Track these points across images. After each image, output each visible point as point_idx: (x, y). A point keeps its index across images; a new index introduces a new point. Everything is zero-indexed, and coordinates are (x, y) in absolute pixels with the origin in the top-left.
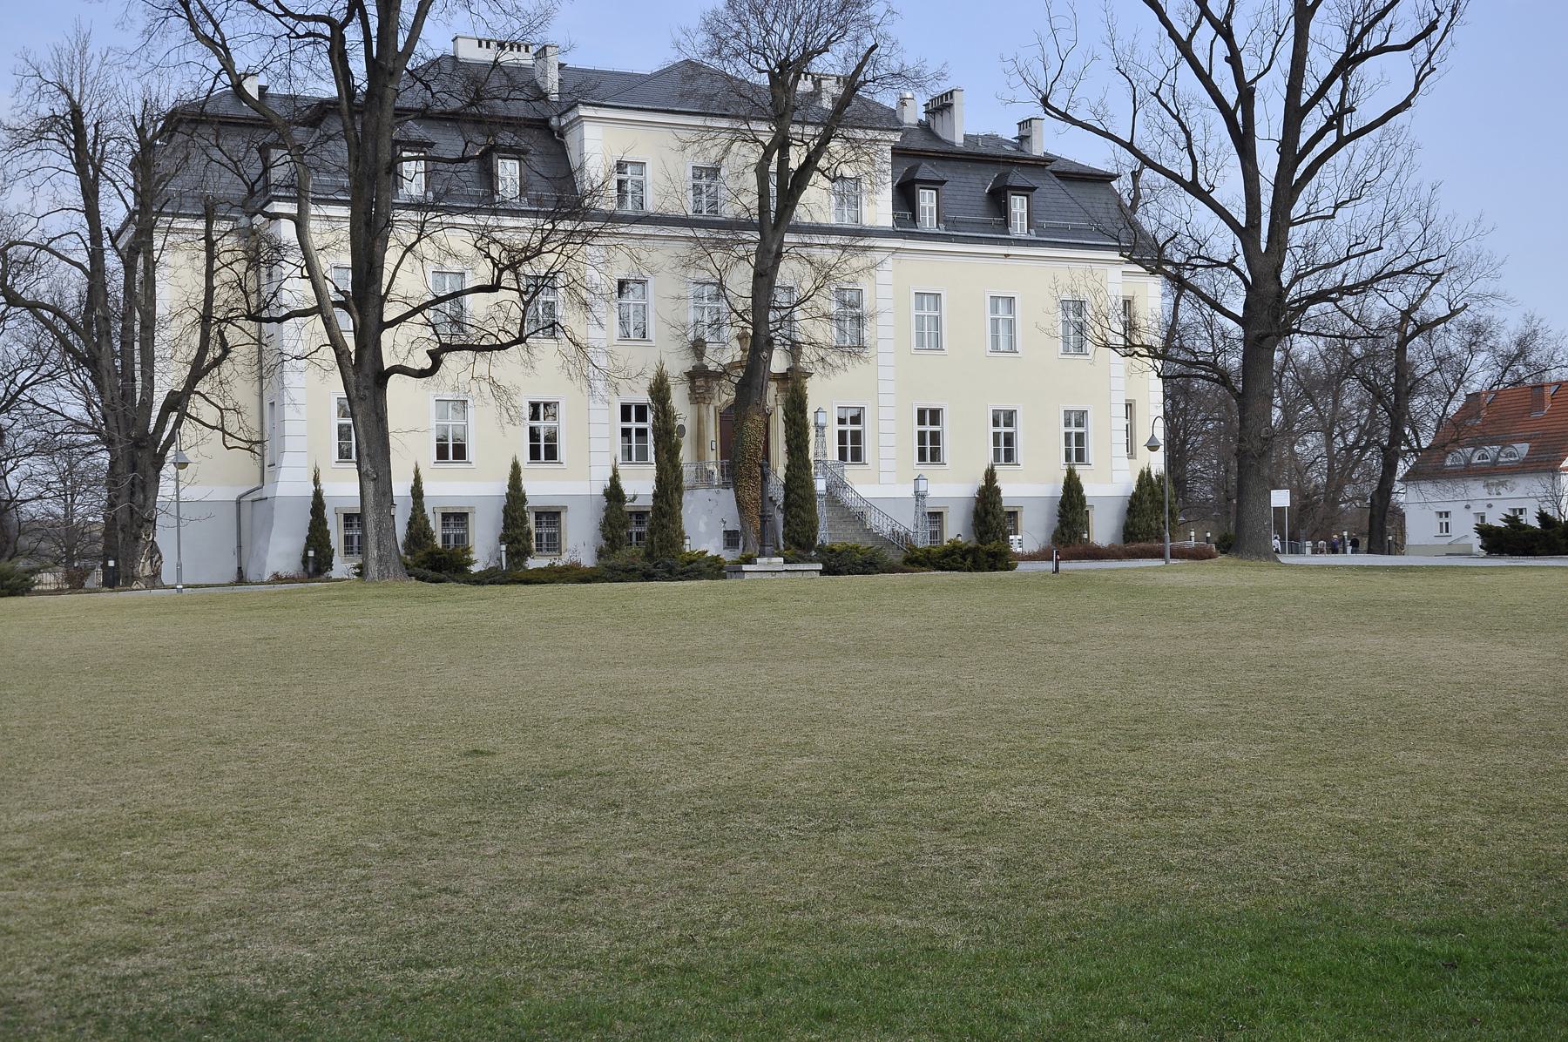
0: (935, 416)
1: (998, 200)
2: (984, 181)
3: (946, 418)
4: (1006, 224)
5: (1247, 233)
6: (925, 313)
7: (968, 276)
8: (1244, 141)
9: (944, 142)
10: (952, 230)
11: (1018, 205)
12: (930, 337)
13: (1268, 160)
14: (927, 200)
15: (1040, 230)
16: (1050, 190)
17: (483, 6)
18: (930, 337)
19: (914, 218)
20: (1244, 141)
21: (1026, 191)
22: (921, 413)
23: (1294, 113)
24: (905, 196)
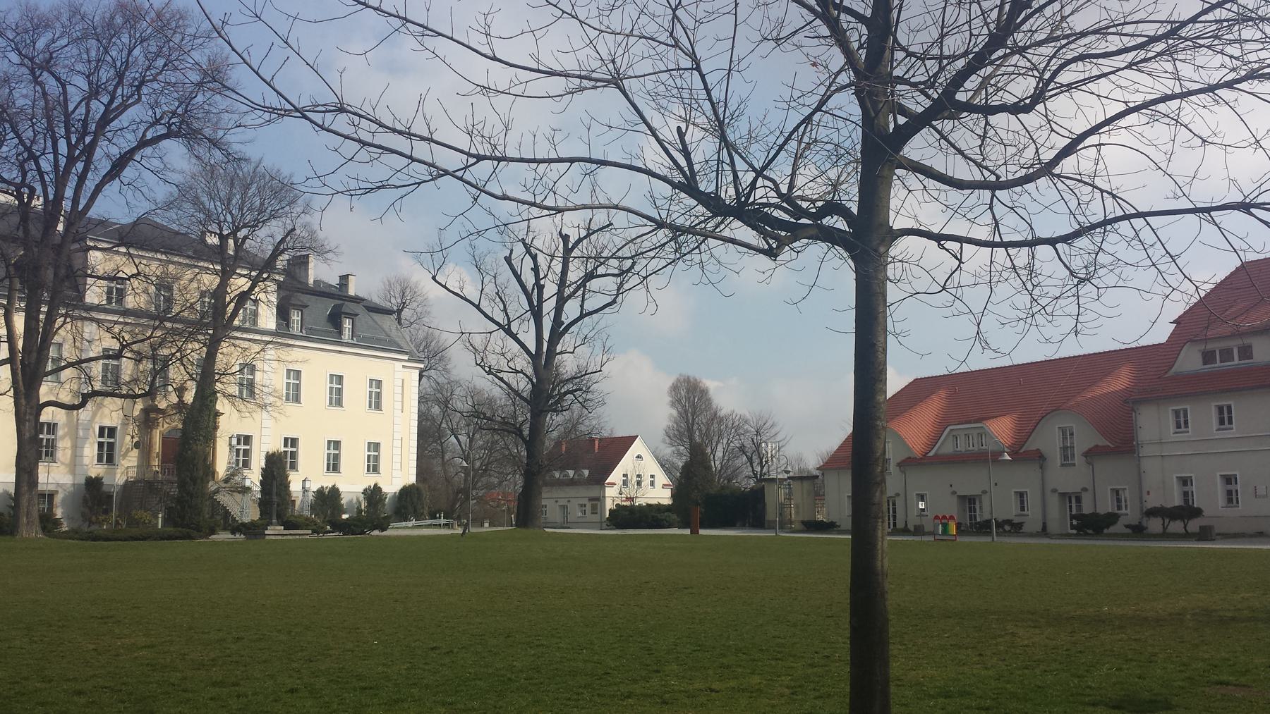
0: (377, 446)
1: (335, 320)
2: (328, 306)
3: (301, 444)
4: (340, 333)
5: (535, 358)
6: (292, 381)
7: (318, 363)
8: (537, 314)
9: (300, 282)
10: (311, 335)
11: (347, 324)
12: (337, 398)
13: (547, 324)
14: (296, 317)
15: (310, 330)
16: (364, 317)
17: (4, 149)
18: (337, 398)
19: (288, 325)
20: (537, 314)
21: (353, 316)
22: (286, 439)
23: (561, 300)
24: (283, 314)
